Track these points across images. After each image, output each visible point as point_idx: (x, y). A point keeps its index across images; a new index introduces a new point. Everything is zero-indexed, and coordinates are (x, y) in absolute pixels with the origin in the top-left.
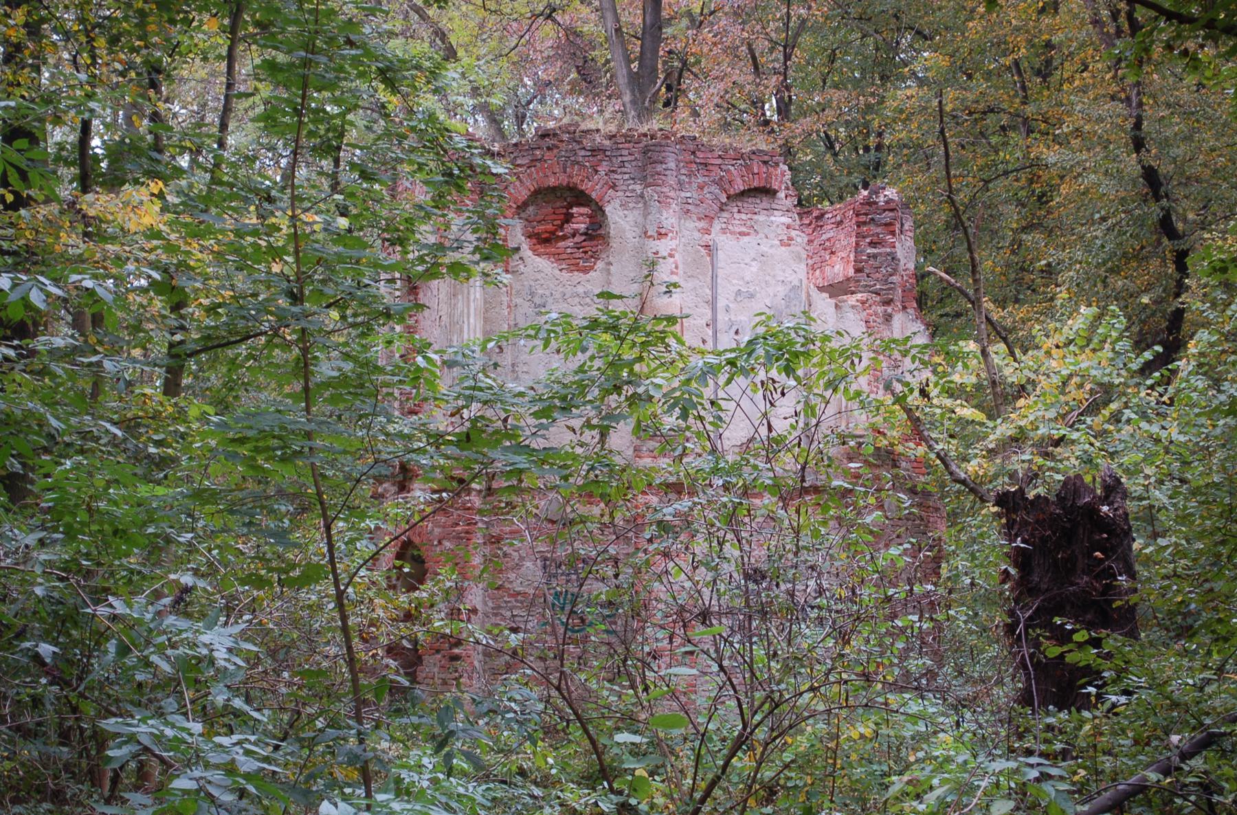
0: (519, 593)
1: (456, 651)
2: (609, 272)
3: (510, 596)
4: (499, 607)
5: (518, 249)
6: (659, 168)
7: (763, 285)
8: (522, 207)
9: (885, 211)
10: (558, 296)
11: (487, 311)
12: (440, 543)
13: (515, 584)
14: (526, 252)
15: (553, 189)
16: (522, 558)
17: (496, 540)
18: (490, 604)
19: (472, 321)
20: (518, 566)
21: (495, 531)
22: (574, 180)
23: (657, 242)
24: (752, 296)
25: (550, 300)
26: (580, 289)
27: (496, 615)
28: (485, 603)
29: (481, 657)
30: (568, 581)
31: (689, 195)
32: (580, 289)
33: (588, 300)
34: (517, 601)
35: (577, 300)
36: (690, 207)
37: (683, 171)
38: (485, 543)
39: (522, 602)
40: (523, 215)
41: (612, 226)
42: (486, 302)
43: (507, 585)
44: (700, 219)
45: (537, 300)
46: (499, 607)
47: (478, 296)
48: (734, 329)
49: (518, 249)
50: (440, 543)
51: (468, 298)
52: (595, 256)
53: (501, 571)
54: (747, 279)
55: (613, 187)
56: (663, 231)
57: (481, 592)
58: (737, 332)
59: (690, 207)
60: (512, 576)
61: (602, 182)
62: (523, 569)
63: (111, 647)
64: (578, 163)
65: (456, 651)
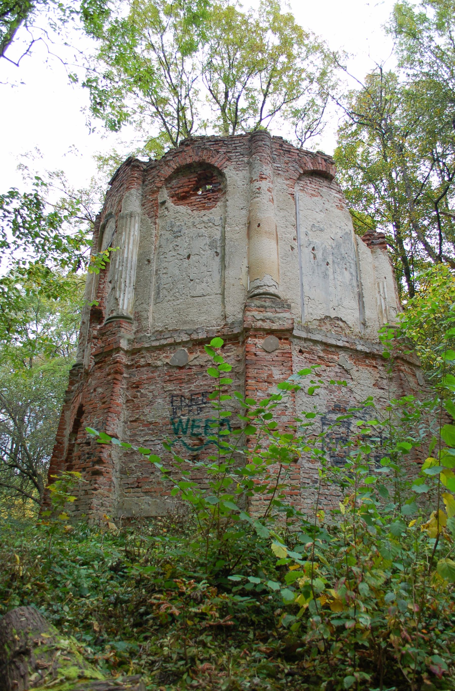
0: (151, 423)
1: (97, 467)
2: (226, 206)
3: (144, 425)
4: (135, 435)
5: (164, 203)
6: (260, 143)
7: (329, 226)
8: (169, 180)
9: (379, 238)
10: (190, 224)
11: (141, 242)
12: (95, 390)
13: (148, 417)
14: (170, 204)
15: (189, 166)
16: (155, 397)
17: (137, 386)
18: (128, 433)
19: (131, 247)
20: (151, 403)
21: (136, 379)
22: (204, 158)
23: (259, 182)
24: (322, 230)
25: (184, 227)
26: (205, 219)
27: (132, 441)
28: (125, 433)
29: (118, 474)
30: (190, 411)
31: (279, 165)
32: (205, 219)
33: (210, 224)
34: (149, 429)
35: (203, 225)
36: (280, 172)
37: (275, 153)
38: (127, 388)
39: (153, 430)
40: (169, 185)
41: (228, 179)
42: (141, 237)
43: (142, 418)
44: (287, 179)
45: (175, 229)
46: (135, 435)
47: (136, 233)
48: (312, 246)
49: (164, 203)
50: (95, 390)
51: (129, 234)
52: (216, 200)
53: (138, 408)
54: (318, 220)
55: (229, 159)
56: (264, 176)
57: (122, 424)
58: (313, 249)
59: (280, 172)
60: (146, 410)
61: (222, 157)
62: (156, 404)
63: (169, 666)
64: (206, 149)
65: (97, 467)
